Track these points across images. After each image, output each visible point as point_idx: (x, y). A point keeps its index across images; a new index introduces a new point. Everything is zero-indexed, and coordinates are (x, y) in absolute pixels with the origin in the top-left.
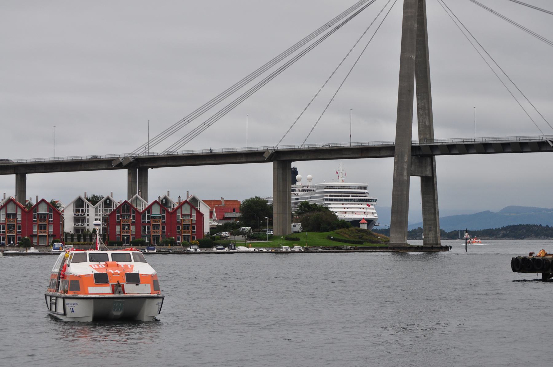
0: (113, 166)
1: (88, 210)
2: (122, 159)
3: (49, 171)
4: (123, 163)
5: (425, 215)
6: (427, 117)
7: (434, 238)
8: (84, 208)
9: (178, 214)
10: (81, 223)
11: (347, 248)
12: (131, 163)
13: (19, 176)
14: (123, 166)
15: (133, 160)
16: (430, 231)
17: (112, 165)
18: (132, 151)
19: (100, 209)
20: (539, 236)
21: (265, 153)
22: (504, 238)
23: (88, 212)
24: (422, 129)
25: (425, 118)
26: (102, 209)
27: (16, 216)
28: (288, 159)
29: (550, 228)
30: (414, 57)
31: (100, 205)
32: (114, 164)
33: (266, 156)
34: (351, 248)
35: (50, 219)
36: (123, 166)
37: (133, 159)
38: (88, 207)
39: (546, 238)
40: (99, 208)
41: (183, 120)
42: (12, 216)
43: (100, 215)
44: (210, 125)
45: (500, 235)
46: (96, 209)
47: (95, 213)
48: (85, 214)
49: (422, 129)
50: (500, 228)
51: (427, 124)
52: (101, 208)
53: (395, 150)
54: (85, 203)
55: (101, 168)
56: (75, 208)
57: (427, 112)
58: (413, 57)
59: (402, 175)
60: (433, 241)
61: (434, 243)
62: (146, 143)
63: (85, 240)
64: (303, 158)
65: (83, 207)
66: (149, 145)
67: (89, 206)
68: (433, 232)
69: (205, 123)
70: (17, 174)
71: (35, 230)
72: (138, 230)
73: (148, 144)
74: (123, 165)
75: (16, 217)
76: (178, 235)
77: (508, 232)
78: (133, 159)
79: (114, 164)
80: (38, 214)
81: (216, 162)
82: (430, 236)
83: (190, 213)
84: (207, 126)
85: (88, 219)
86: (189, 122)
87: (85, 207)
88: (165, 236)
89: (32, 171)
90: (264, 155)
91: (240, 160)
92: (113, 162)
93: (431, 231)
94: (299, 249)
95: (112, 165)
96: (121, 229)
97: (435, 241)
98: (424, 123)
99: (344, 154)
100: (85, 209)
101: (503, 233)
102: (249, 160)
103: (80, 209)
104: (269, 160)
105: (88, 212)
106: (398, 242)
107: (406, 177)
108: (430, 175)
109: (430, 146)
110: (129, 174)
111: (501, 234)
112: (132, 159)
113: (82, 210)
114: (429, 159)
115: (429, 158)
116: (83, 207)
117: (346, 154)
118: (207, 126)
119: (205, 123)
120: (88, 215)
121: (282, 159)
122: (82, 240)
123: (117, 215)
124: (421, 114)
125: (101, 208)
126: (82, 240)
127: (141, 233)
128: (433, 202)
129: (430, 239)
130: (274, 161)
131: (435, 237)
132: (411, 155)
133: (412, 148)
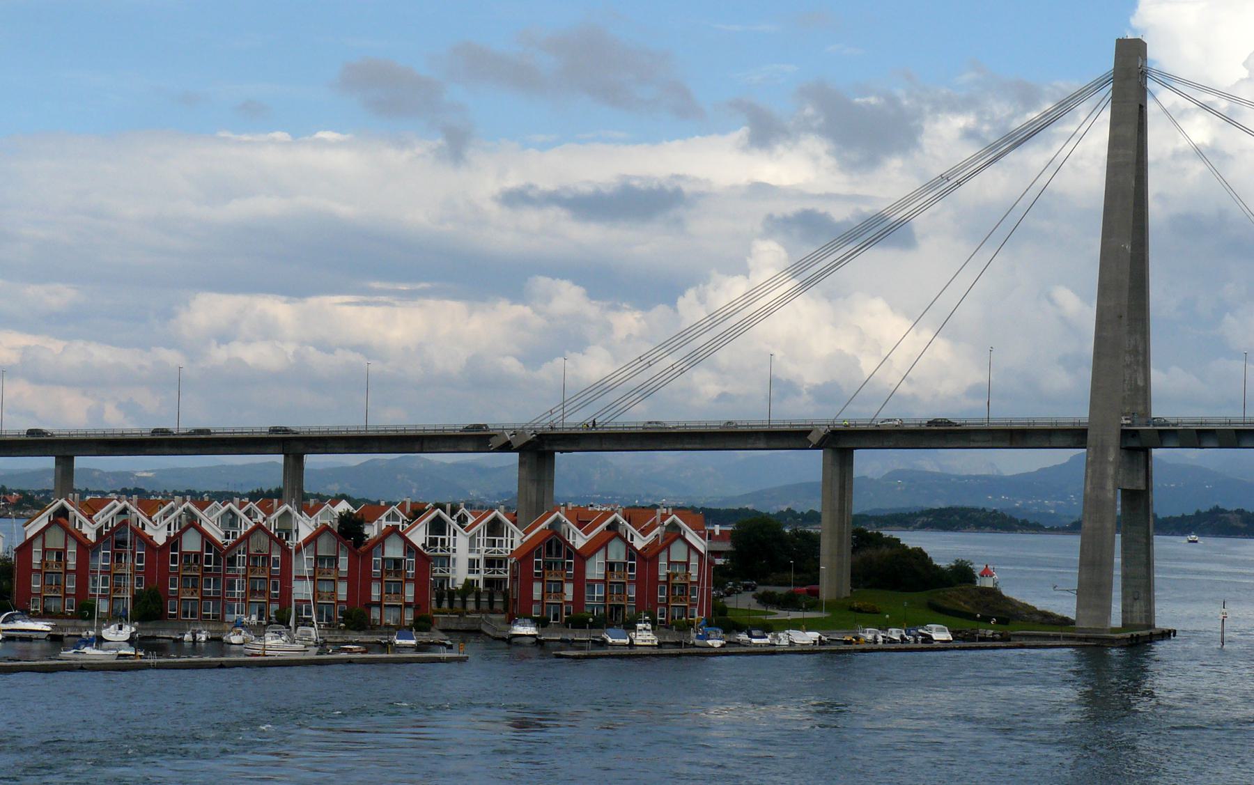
0: (491, 447)
1: (455, 540)
2: (512, 435)
3: (354, 451)
4: (512, 442)
5: (1127, 567)
6: (1141, 369)
7: (1143, 615)
8: (446, 537)
9: (663, 562)
10: (438, 568)
11: (985, 634)
12: (529, 442)
13: (291, 459)
14: (512, 449)
15: (534, 438)
16: (1135, 599)
17: (490, 445)
18: (533, 419)
19: (479, 540)
20: (982, 527)
21: (811, 434)
22: (924, 528)
23: (454, 545)
24: (1129, 393)
25: (1135, 371)
26: (484, 540)
27: (337, 563)
28: (847, 446)
29: (999, 515)
30: (1128, 247)
31: (479, 532)
32: (495, 443)
33: (814, 438)
34: (993, 634)
35: (409, 570)
36: (512, 449)
37: (534, 435)
38: (455, 534)
39: (993, 531)
40: (477, 538)
41: (639, 360)
42: (328, 562)
43: (478, 551)
44: (684, 369)
45: (917, 525)
46: (472, 539)
47: (470, 546)
48: (449, 550)
49: (1129, 393)
50: (918, 512)
51: (1140, 383)
52: (481, 538)
53: (1089, 437)
54: (450, 526)
55: (463, 449)
56: (428, 536)
57: (1141, 358)
58: (1127, 247)
59: (1102, 488)
60: (1141, 619)
61: (1144, 622)
62: (559, 406)
63: (451, 606)
64: (886, 444)
65: (445, 535)
66: (565, 410)
67: (458, 533)
68: (1142, 604)
69: (674, 366)
70: (286, 455)
71: (375, 593)
72: (578, 593)
73: (562, 406)
74: (512, 447)
75: (336, 566)
76: (661, 604)
77: (930, 519)
78: (534, 435)
79: (495, 443)
80: (383, 560)
81: (703, 447)
82: (1134, 609)
83: (686, 560)
84: (679, 373)
85: (454, 560)
86: (650, 365)
87: (449, 535)
88: (635, 606)
89: (319, 450)
90: (808, 437)
91: (753, 444)
92: (492, 440)
93: (1138, 599)
94: (900, 634)
95: (490, 445)
96: (543, 590)
97: (1146, 620)
98: (1133, 382)
99: (974, 441)
100: (449, 539)
101: (922, 519)
102: (773, 444)
103: (399, 521)
104: (816, 447)
105: (454, 545)
106: (1093, 627)
107: (1112, 492)
108: (1143, 488)
109: (1159, 430)
110: (521, 463)
111: (919, 523)
112: (532, 434)
113: (443, 541)
114: (1142, 455)
115: (1142, 453)
116: (445, 535)
117: (977, 442)
118: (679, 373)
119: (674, 366)
120: (454, 551)
121: (840, 446)
122: (445, 605)
123: (535, 560)
124: (1129, 363)
125: (481, 538)
126: (445, 605)
127: (586, 600)
128: (1145, 541)
129: (1134, 615)
130: (825, 449)
131: (1145, 612)
132: (1121, 448)
133: (1083, 429)
